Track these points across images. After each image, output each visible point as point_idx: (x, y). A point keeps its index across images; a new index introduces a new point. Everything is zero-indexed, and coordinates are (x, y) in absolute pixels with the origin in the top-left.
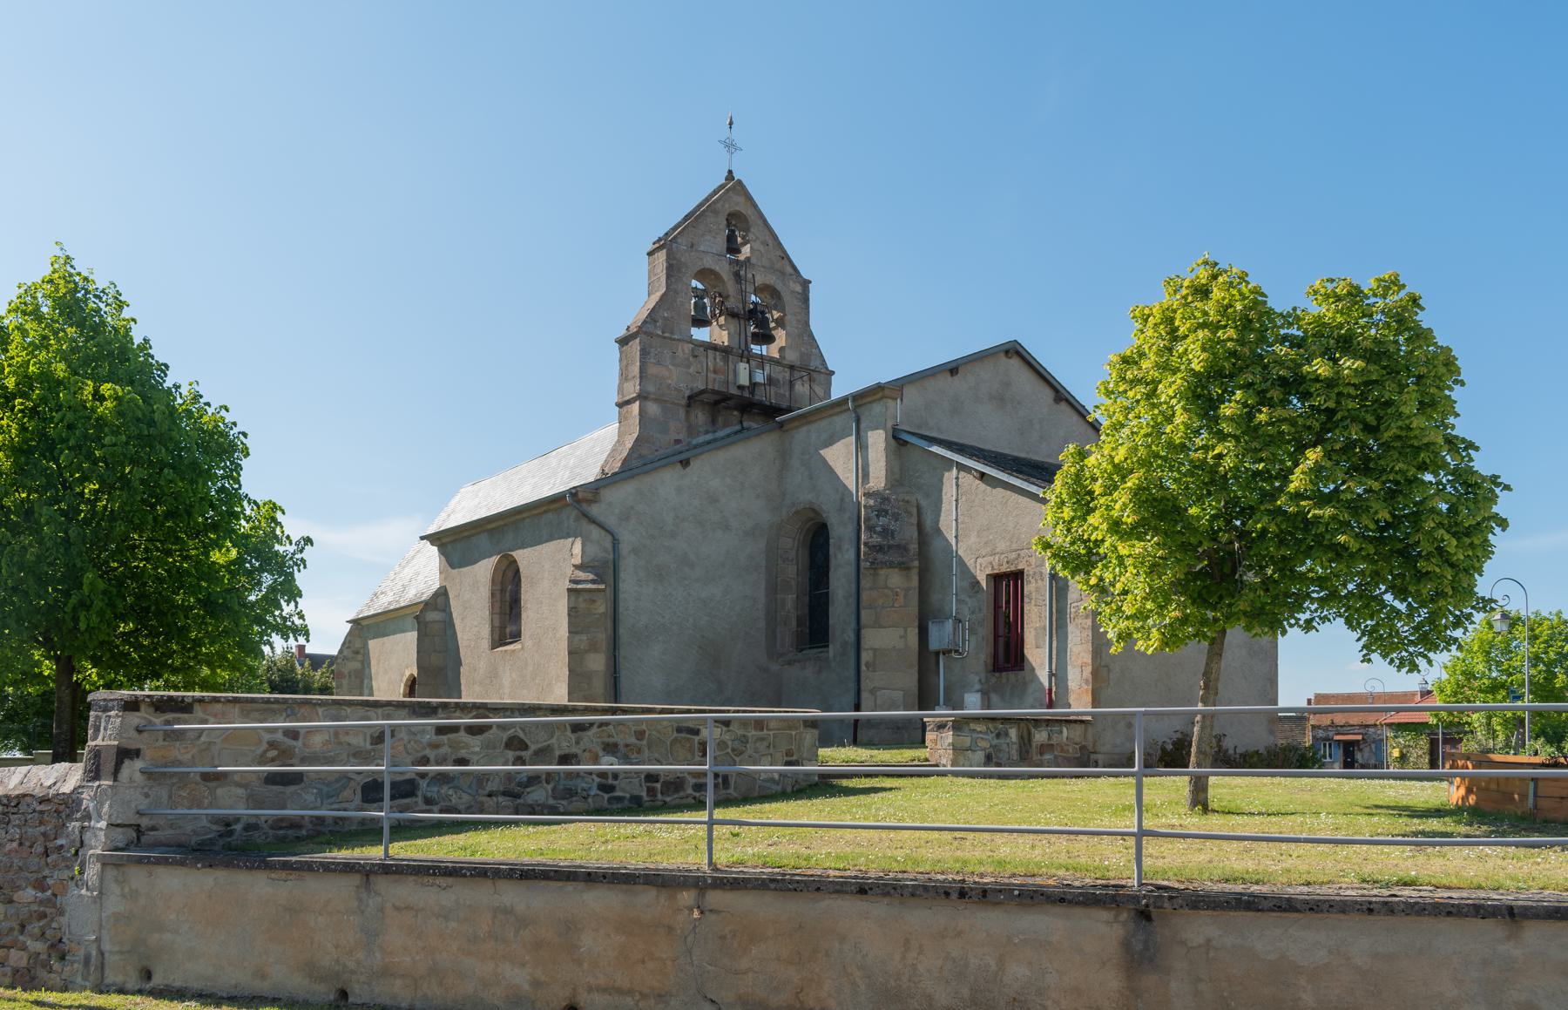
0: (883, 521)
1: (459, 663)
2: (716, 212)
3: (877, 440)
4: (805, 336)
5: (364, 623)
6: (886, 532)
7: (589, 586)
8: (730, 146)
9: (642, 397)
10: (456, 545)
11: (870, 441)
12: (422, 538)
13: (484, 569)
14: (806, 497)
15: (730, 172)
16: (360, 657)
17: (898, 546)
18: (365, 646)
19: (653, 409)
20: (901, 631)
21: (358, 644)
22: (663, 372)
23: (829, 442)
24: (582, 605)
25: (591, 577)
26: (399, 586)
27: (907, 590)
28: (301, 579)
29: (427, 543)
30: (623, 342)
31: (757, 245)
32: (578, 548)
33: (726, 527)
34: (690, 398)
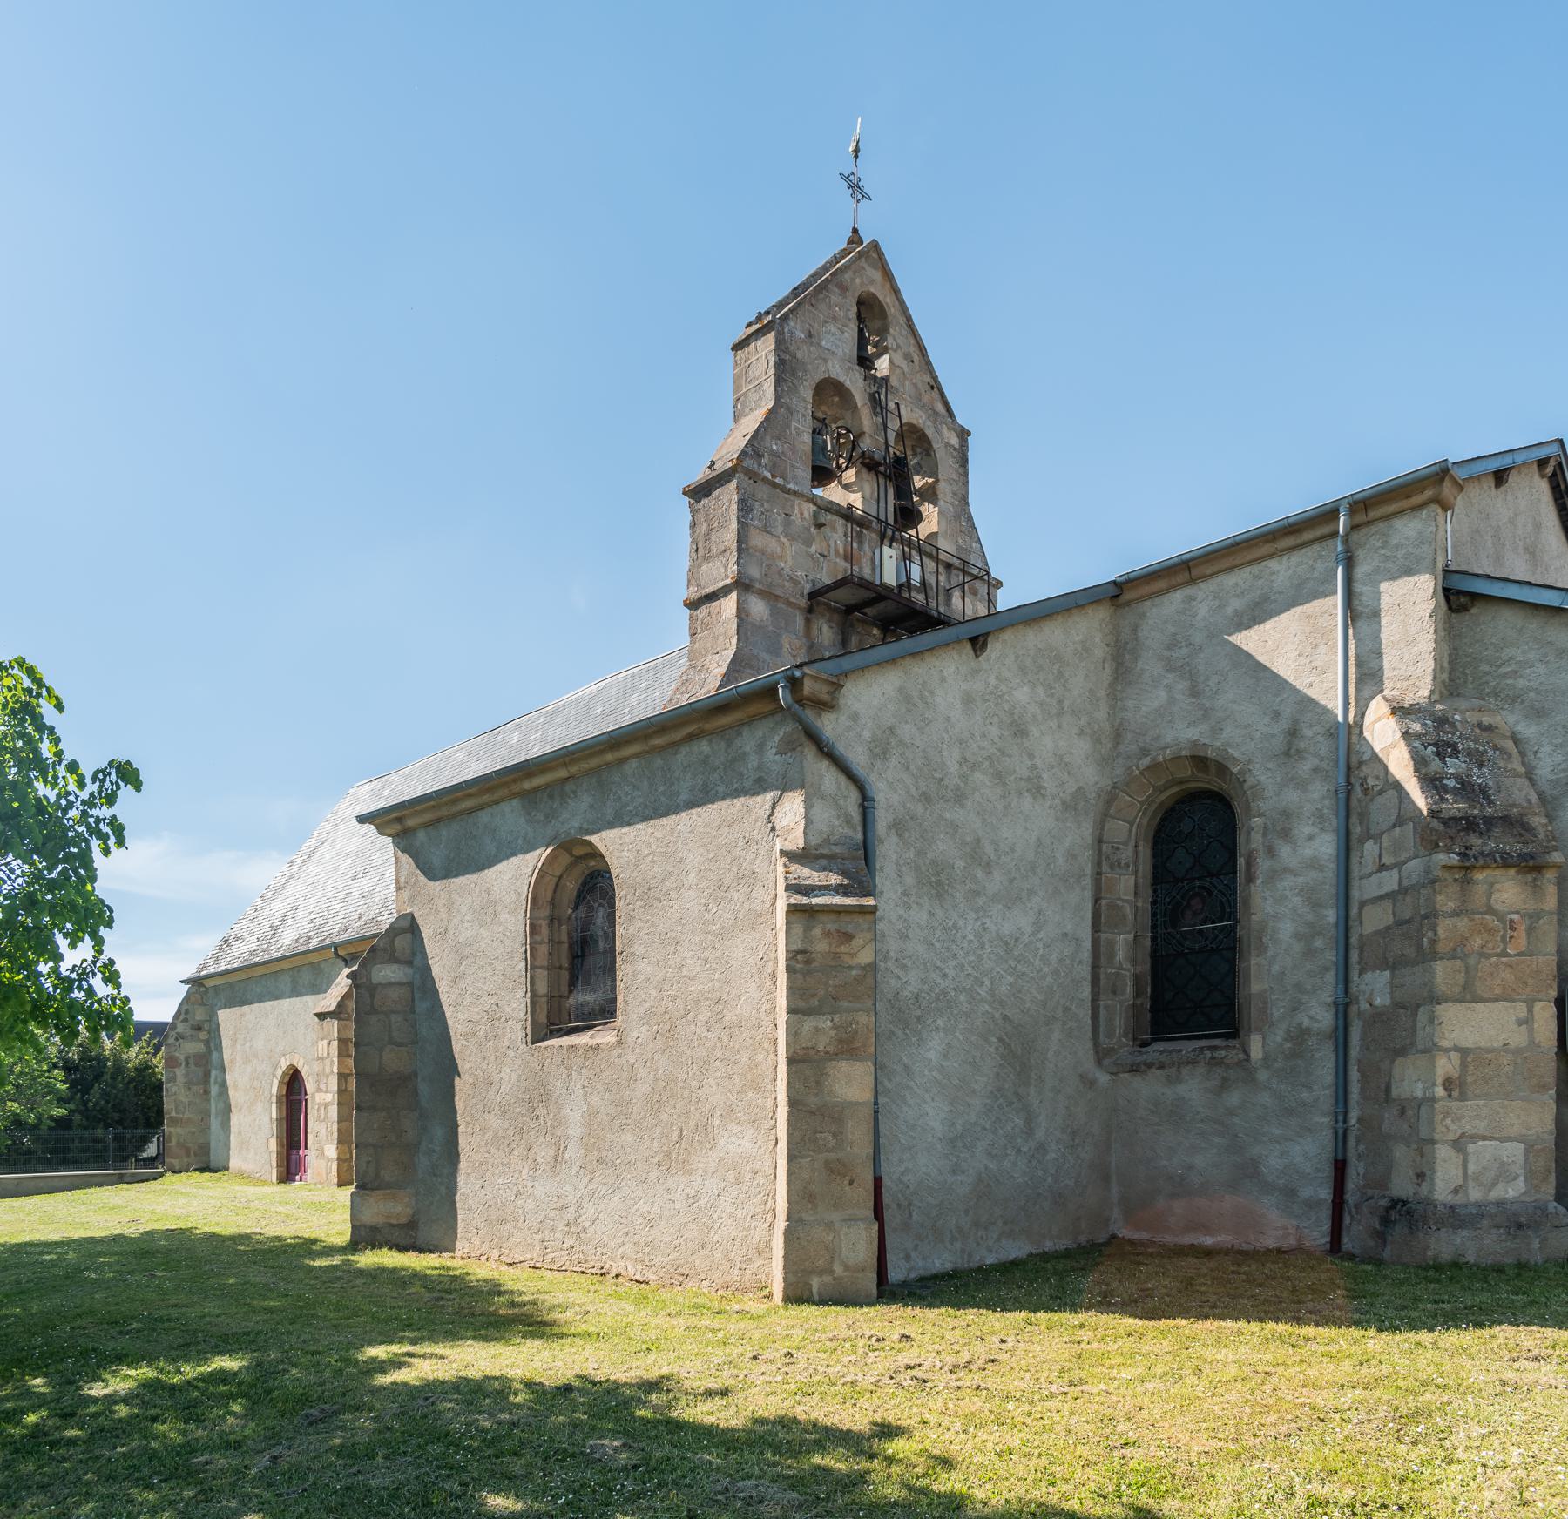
0: (1454, 766)
1: (450, 1069)
2: (843, 289)
3: (1408, 608)
4: (962, 517)
5: (210, 983)
6: (1466, 788)
7: (837, 900)
8: (855, 187)
9: (742, 585)
10: (438, 830)
11: (1386, 601)
12: (362, 819)
13: (513, 879)
14: (1182, 733)
15: (855, 231)
16: (203, 1035)
17: (1506, 820)
18: (212, 1018)
19: (758, 607)
20: (1521, 1009)
21: (199, 1015)
22: (773, 546)
23: (1257, 613)
24: (821, 946)
25: (834, 879)
26: (266, 926)
27: (1534, 917)
28: (113, 874)
29: (370, 828)
30: (699, 492)
31: (899, 360)
32: (792, 810)
33: (1038, 791)
34: (813, 596)
